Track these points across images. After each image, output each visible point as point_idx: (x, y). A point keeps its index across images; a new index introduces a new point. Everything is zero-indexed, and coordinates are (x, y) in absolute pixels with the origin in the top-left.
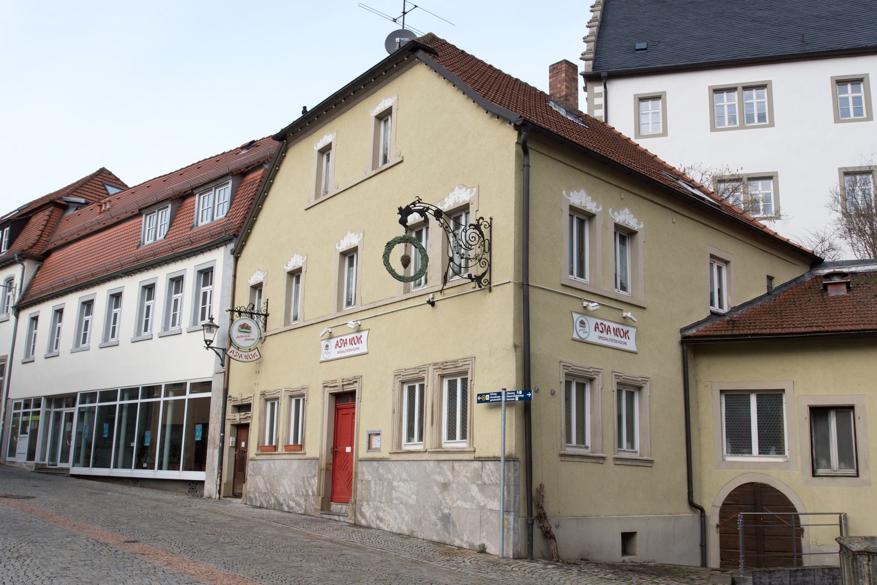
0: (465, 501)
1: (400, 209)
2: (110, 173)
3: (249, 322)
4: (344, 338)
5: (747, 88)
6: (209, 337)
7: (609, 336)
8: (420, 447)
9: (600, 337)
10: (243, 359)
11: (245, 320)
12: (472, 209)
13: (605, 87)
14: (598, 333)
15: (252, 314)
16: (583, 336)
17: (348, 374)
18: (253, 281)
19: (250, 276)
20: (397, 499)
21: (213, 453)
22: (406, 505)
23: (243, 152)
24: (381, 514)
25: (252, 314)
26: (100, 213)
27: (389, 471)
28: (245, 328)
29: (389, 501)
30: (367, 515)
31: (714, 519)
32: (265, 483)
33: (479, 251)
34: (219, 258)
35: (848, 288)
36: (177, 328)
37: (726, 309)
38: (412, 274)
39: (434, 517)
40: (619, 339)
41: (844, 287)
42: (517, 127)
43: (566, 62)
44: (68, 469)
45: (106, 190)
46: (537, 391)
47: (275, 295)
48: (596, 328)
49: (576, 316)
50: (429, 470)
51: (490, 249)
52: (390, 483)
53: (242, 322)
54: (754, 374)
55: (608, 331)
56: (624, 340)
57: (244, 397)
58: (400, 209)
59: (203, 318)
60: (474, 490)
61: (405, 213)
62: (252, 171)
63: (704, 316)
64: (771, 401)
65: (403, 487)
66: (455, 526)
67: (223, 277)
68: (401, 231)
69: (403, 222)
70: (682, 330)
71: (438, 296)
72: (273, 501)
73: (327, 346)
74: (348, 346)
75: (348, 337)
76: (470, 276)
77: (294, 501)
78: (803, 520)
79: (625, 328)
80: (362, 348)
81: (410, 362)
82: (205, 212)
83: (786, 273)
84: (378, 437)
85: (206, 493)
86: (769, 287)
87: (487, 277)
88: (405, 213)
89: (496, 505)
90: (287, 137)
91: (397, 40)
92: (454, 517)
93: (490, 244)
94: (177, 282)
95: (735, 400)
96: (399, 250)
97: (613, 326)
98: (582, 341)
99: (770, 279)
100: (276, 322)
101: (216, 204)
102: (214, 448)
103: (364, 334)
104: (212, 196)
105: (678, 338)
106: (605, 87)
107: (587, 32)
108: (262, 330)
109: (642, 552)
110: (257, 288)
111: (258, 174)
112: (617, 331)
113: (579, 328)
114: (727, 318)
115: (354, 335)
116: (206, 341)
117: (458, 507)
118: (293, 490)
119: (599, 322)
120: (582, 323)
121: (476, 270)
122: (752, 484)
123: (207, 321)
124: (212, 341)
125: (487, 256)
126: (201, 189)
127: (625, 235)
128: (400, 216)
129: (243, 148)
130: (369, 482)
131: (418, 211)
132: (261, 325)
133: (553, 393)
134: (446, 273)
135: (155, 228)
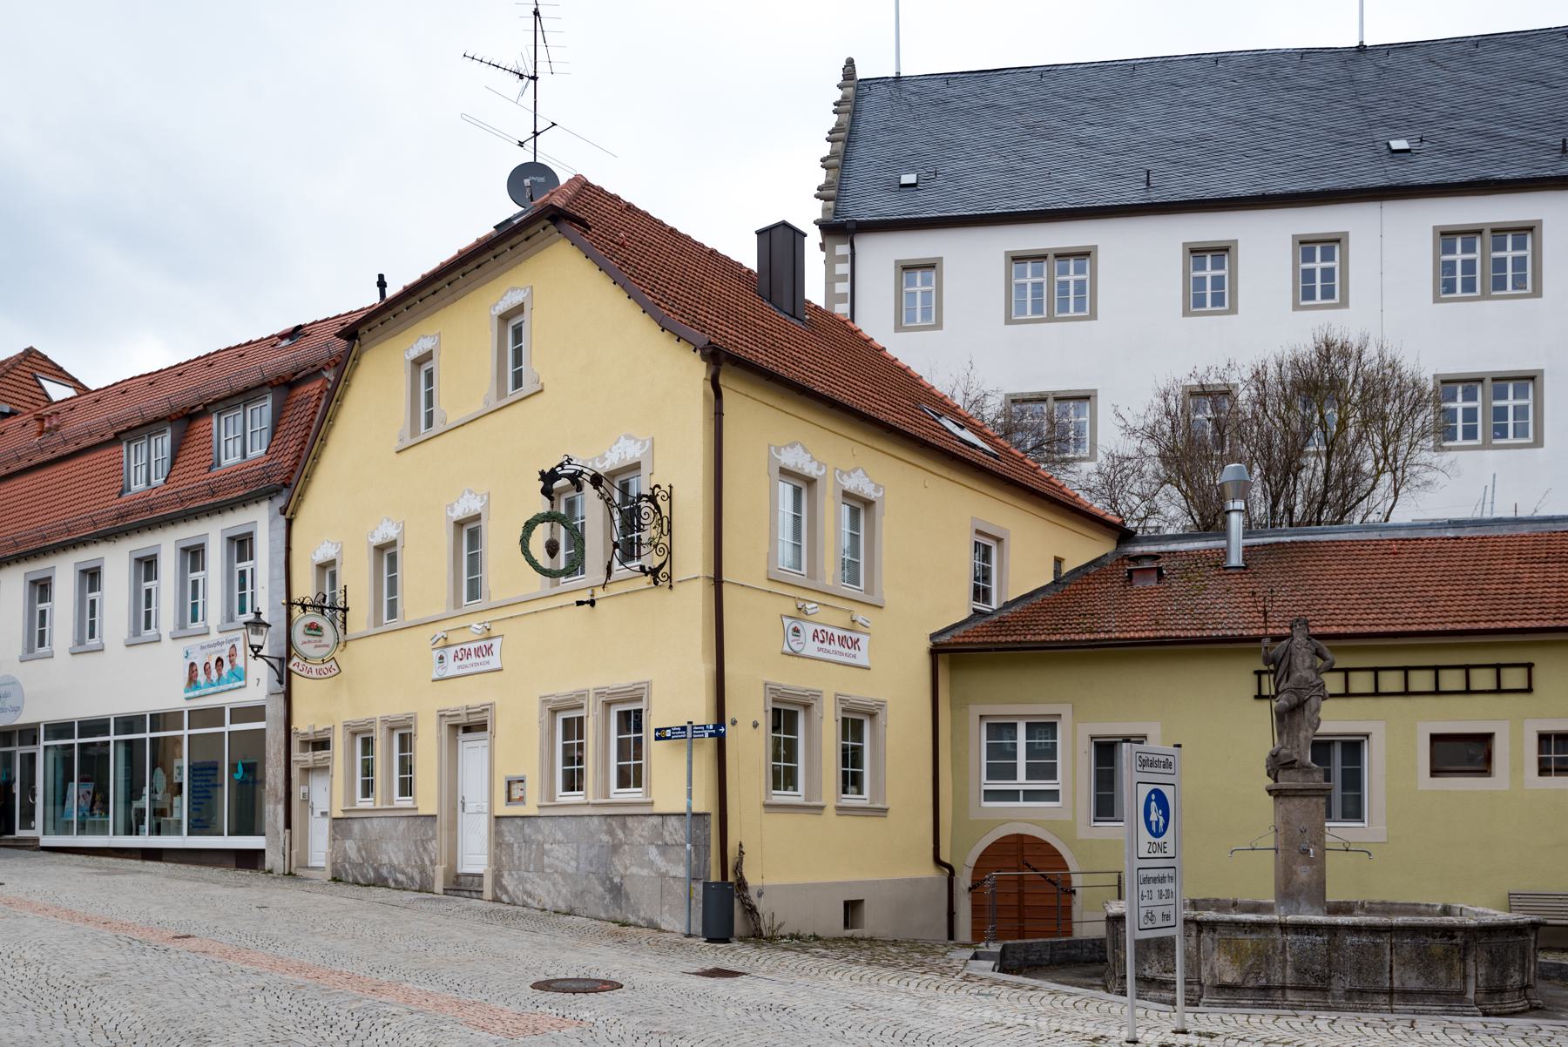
0: (642, 866)
1: (542, 473)
2: (45, 358)
3: (322, 622)
4: (466, 647)
5: (1062, 256)
6: (256, 640)
7: (832, 647)
8: (580, 799)
9: (820, 650)
10: (314, 675)
11: (312, 617)
12: (645, 470)
13: (852, 247)
14: (817, 644)
15: (322, 608)
16: (797, 648)
17: (475, 701)
18: (322, 556)
19: (311, 547)
20: (550, 866)
21: (276, 815)
22: (564, 874)
23: (285, 343)
24: (529, 887)
25: (322, 608)
26: (41, 433)
27: (538, 830)
28: (313, 628)
29: (540, 870)
30: (510, 889)
31: (964, 880)
32: (359, 850)
33: (654, 533)
34: (260, 519)
35: (1160, 576)
36: (199, 625)
37: (994, 605)
38: (562, 566)
39: (601, 889)
40: (846, 650)
41: (1154, 575)
42: (704, 357)
43: (784, 224)
44: (37, 840)
45: (41, 387)
46: (734, 723)
47: (357, 581)
48: (815, 636)
49: (787, 622)
50: (592, 827)
51: (670, 530)
52: (540, 845)
53: (308, 621)
54: (1021, 696)
55: (831, 640)
56: (852, 651)
57: (318, 728)
58: (542, 473)
59: (242, 611)
60: (653, 853)
61: (549, 478)
62: (301, 381)
63: (964, 616)
64: (1043, 729)
65: (558, 851)
66: (628, 898)
67: (271, 548)
68: (543, 505)
69: (547, 492)
70: (933, 636)
71: (599, 593)
72: (372, 874)
73: (441, 658)
74: (473, 659)
75: (473, 646)
76: (642, 568)
77: (403, 873)
78: (1076, 881)
79: (855, 636)
80: (494, 661)
81: (564, 688)
82: (230, 443)
83: (1082, 549)
84: (520, 785)
85: (268, 866)
86: (1057, 572)
87: (666, 569)
88: (549, 478)
89: (681, 871)
90: (357, 331)
91: (527, 182)
92: (628, 886)
93: (670, 523)
94: (194, 555)
95: (1001, 730)
96: (541, 534)
97: (837, 633)
98: (795, 654)
99: (1058, 561)
100: (360, 618)
101: (249, 431)
102: (277, 803)
103: (496, 643)
104: (240, 419)
105: (928, 644)
106: (852, 247)
107: (826, 149)
108: (341, 631)
109: (872, 922)
110: (327, 569)
111: (313, 388)
112: (842, 640)
113: (791, 637)
114: (996, 618)
115: (481, 644)
116: (252, 647)
117: (633, 875)
118: (402, 858)
119: (819, 628)
120: (796, 630)
121: (651, 559)
122: (1020, 837)
123: (250, 616)
124: (260, 647)
125: (665, 540)
126: (221, 405)
127: (860, 506)
128: (541, 484)
129: (282, 336)
130: (510, 846)
131: (568, 476)
132: (338, 624)
133: (755, 725)
134: (610, 563)
135: (146, 467)
